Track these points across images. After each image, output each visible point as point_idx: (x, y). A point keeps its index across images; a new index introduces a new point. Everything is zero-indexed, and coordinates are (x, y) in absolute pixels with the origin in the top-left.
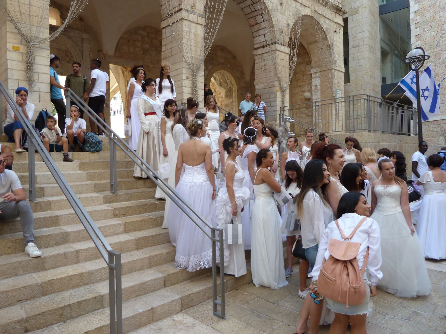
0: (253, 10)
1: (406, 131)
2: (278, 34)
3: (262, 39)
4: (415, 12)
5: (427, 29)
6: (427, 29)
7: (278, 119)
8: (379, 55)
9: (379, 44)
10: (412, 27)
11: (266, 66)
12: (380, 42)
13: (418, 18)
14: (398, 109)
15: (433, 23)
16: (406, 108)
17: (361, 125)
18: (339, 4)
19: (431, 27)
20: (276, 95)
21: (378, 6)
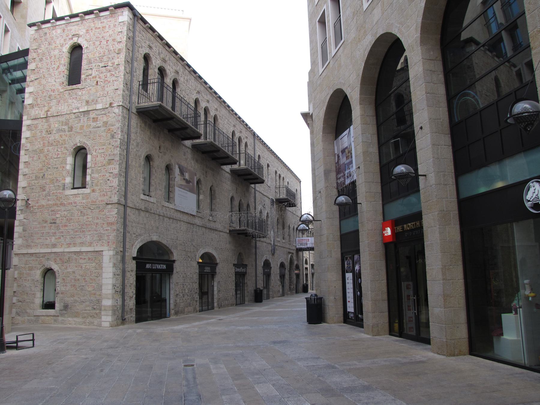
4: (27, 138)
6: (35, 159)
10: (22, 152)
13: (29, 145)
15: (41, 155)
19: (39, 158)
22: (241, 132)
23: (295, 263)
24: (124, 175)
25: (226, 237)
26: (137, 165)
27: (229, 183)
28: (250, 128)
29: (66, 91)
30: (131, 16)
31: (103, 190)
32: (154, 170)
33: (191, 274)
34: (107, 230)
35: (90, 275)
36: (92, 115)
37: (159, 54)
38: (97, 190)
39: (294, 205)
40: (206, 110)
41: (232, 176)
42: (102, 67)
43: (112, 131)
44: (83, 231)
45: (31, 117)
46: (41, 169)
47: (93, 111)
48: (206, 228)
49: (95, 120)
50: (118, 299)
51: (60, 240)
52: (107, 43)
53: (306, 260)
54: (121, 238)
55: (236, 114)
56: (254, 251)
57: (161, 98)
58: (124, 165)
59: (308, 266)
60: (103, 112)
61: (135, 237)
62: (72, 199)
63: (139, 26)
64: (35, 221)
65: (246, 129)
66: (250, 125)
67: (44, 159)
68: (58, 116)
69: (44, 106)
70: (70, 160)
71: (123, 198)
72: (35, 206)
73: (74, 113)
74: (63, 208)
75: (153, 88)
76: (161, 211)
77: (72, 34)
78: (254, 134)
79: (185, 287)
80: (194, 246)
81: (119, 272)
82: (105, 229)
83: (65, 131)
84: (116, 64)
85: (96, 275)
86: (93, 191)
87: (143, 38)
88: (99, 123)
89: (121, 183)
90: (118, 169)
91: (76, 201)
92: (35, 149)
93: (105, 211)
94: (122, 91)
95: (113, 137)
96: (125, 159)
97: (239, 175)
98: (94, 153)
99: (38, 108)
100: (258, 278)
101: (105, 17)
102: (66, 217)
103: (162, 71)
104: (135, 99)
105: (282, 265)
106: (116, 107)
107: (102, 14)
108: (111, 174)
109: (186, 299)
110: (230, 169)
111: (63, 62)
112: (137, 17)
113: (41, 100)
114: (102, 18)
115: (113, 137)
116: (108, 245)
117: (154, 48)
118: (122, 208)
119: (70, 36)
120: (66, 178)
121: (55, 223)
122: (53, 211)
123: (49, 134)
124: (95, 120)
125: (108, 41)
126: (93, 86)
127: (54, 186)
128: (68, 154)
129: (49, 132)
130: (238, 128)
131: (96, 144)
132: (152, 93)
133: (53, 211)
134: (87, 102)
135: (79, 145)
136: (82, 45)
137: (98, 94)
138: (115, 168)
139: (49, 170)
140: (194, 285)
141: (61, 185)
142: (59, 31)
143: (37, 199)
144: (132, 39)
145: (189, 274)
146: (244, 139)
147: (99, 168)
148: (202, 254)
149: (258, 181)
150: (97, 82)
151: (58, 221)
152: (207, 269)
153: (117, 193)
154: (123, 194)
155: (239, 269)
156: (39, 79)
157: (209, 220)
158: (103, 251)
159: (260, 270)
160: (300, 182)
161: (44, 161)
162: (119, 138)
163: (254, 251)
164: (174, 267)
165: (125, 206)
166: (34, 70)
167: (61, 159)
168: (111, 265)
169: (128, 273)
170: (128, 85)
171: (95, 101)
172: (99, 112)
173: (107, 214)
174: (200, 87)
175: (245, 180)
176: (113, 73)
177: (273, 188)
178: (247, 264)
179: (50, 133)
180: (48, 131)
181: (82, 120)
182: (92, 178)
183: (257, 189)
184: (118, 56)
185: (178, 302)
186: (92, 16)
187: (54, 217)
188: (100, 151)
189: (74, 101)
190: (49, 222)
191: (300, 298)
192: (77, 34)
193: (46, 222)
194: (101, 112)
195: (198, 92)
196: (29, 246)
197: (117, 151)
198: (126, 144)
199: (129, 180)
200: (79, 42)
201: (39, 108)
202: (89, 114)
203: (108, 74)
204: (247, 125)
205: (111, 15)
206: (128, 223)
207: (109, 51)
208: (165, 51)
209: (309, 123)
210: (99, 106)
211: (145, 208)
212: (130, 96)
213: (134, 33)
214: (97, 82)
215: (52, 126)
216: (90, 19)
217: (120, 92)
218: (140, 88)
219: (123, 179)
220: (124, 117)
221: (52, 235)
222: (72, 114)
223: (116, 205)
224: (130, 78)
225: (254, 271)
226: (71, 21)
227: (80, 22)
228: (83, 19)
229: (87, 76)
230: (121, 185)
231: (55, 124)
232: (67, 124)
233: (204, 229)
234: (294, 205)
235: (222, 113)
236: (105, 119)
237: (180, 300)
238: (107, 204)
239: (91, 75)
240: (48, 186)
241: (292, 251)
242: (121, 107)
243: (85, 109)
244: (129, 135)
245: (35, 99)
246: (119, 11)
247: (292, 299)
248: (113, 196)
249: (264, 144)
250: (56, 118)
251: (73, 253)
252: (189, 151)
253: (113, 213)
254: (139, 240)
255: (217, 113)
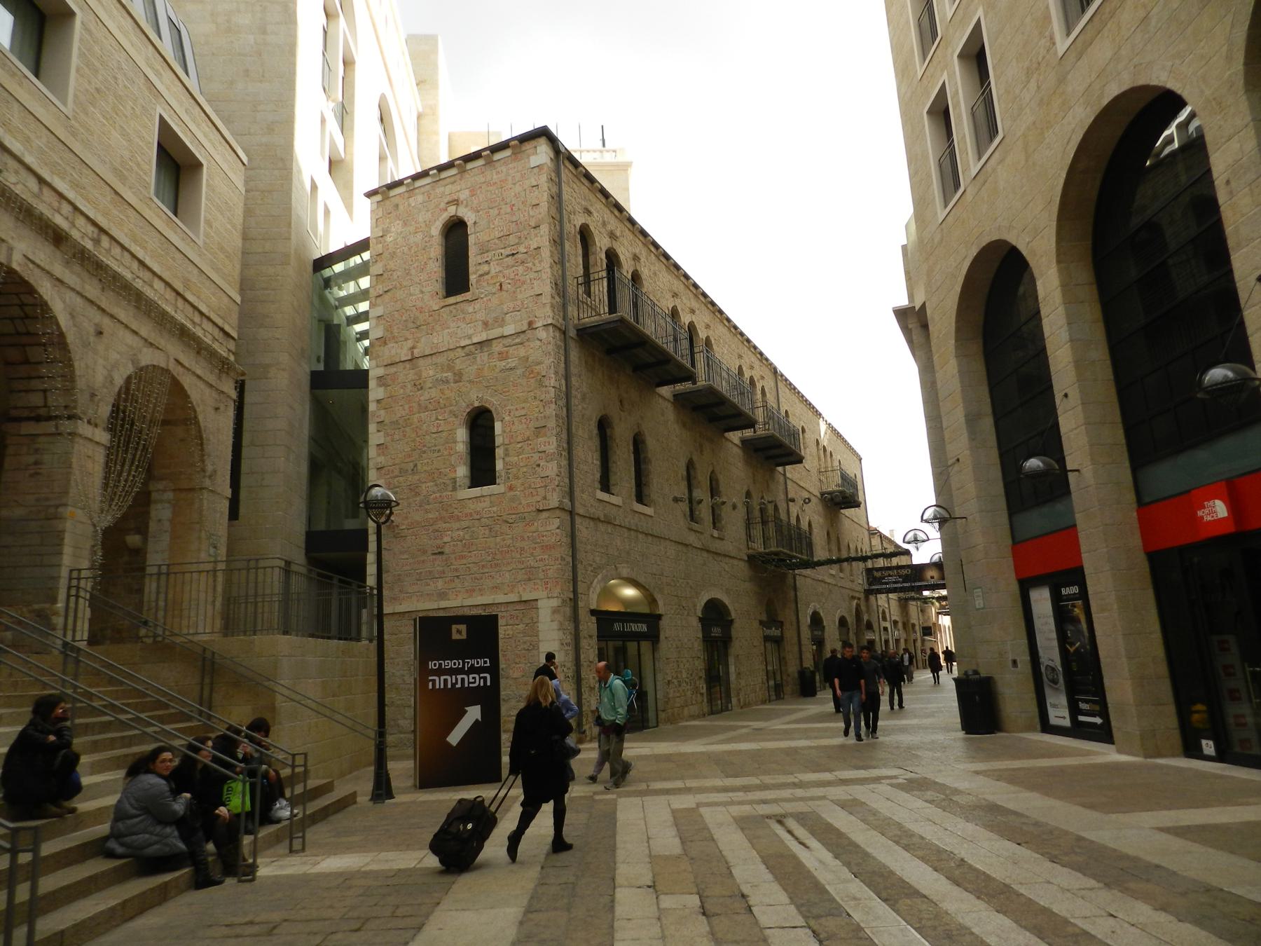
0: (22, 329)
1: (354, 634)
2: (82, 399)
3: (36, 399)
4: (378, 401)
5: (397, 437)
6: (397, 437)
7: (62, 595)
8: (304, 468)
9: (306, 445)
10: (372, 428)
11: (39, 466)
12: (309, 442)
13: (382, 412)
14: (340, 587)
15: (407, 429)
16: (354, 587)
17: (246, 608)
18: (231, 354)
19: (405, 436)
20: (63, 539)
21: (308, 370)
22: (752, 368)
23: (866, 618)
24: (567, 455)
25: (742, 568)
26: (586, 436)
27: (740, 465)
28: (767, 360)
29: (443, 307)
30: (552, 155)
31: (530, 485)
32: (615, 445)
33: (689, 640)
34: (541, 560)
35: (516, 647)
36: (497, 347)
37: (604, 224)
38: (519, 485)
39: (857, 505)
40: (692, 329)
41: (744, 452)
42: (508, 256)
43: (538, 373)
44: (497, 565)
45: (383, 360)
46: (409, 456)
47: (499, 340)
48: (708, 551)
49: (503, 356)
50: (571, 693)
51: (453, 585)
52: (512, 209)
53: (884, 612)
54: (569, 575)
55: (742, 334)
56: (792, 594)
57: (613, 307)
58: (564, 436)
59: (887, 625)
60: (517, 341)
61: (592, 571)
62: (472, 506)
63: (566, 172)
64: (406, 552)
65: (761, 361)
66: (767, 354)
67: (414, 435)
68: (434, 356)
69: (406, 339)
70: (462, 434)
71: (568, 497)
72: (403, 524)
73: (463, 347)
74: (456, 525)
75: (600, 289)
76: (632, 521)
77: (446, 201)
78: (775, 371)
79: (682, 666)
80: (691, 587)
81: (569, 639)
82: (538, 558)
83: (447, 382)
84: (532, 248)
85: (526, 647)
86: (511, 488)
87: (575, 195)
88: (512, 362)
89: (562, 470)
90: (555, 443)
91: (478, 509)
92: (395, 420)
93: (536, 524)
94: (549, 297)
95: (541, 384)
96: (566, 423)
97: (756, 450)
98: (507, 418)
99: (394, 344)
100: (804, 649)
101: (502, 161)
102: (461, 541)
103: (612, 256)
104: (573, 311)
105: (843, 622)
106: (541, 329)
107: (498, 156)
108: (542, 454)
109: (683, 691)
110: (740, 438)
111: (433, 255)
112: (562, 157)
113: (398, 328)
114: (497, 164)
115: (541, 384)
116: (546, 588)
117: (595, 214)
118: (567, 517)
119: (443, 205)
120: (457, 469)
121: (441, 553)
122: (437, 531)
123: (418, 390)
124: (503, 356)
125: (513, 205)
126: (495, 293)
127: (436, 485)
128: (457, 422)
129: (419, 387)
130: (747, 361)
131: (508, 400)
132: (600, 300)
133: (437, 531)
134: (486, 324)
135: (477, 404)
136: (466, 219)
137: (505, 307)
138: (550, 443)
139: (424, 455)
140: (696, 663)
141: (448, 482)
142: (420, 198)
143: (405, 511)
144: (557, 199)
145: (686, 640)
146: (758, 380)
147: (519, 445)
148: (705, 601)
149: (792, 459)
150: (501, 285)
151: (447, 550)
152: (716, 632)
153: (557, 489)
154: (567, 489)
155: (769, 631)
156: (392, 292)
157: (712, 536)
158: (537, 600)
159: (806, 633)
160: (860, 460)
161: (414, 441)
162: (552, 385)
163: (792, 594)
164: (661, 627)
165: (572, 513)
166: (381, 275)
167: (444, 434)
168: (555, 625)
169: (585, 641)
170: (560, 288)
171: (500, 321)
172: (507, 341)
173: (541, 529)
174: (678, 286)
175: (768, 458)
176: (530, 265)
177: (814, 472)
178: (782, 620)
179: (422, 388)
180: (417, 383)
181: (478, 359)
182: (505, 464)
183: (788, 475)
184: (536, 232)
185: (671, 696)
186: (480, 162)
187: (439, 542)
188: (518, 414)
189: (460, 324)
190: (430, 552)
191: (788, 718)
192: (455, 200)
193: (424, 552)
194: (513, 340)
195: (675, 295)
196: (395, 599)
197: (551, 410)
198: (567, 395)
199: (575, 465)
200: (460, 214)
201: (397, 342)
202: (491, 346)
203: (521, 269)
204: (761, 354)
205: (513, 157)
206: (578, 545)
207: (517, 224)
208: (613, 217)
209: (911, 329)
210: (509, 329)
211: (605, 515)
212: (564, 306)
213: (559, 185)
214: (501, 285)
215: (424, 375)
216: (476, 169)
217: (546, 299)
218: (580, 292)
219: (564, 463)
220: (558, 347)
221: (437, 576)
222: (459, 350)
223: (558, 513)
224: (560, 272)
225: (795, 635)
226: (416, 186)
227: (458, 176)
228: (463, 171)
229: (481, 276)
230: (563, 474)
231: (428, 371)
232: (450, 368)
233: (705, 554)
234: (857, 505)
235: (718, 333)
236: (522, 352)
237: (674, 692)
238: (539, 511)
239: (488, 273)
240: (424, 486)
241: (857, 595)
242: (551, 328)
243: (483, 337)
244: (567, 377)
245: (388, 329)
246: (528, 146)
247: (802, 710)
248: (549, 496)
249: (793, 389)
250: (429, 360)
251: (480, 607)
252: (669, 405)
253: (552, 528)
254: (600, 577)
255: (710, 333)
